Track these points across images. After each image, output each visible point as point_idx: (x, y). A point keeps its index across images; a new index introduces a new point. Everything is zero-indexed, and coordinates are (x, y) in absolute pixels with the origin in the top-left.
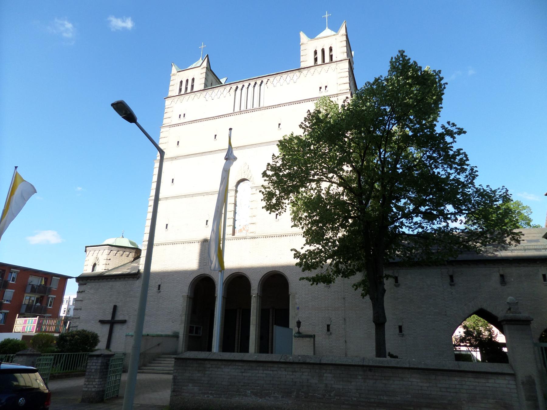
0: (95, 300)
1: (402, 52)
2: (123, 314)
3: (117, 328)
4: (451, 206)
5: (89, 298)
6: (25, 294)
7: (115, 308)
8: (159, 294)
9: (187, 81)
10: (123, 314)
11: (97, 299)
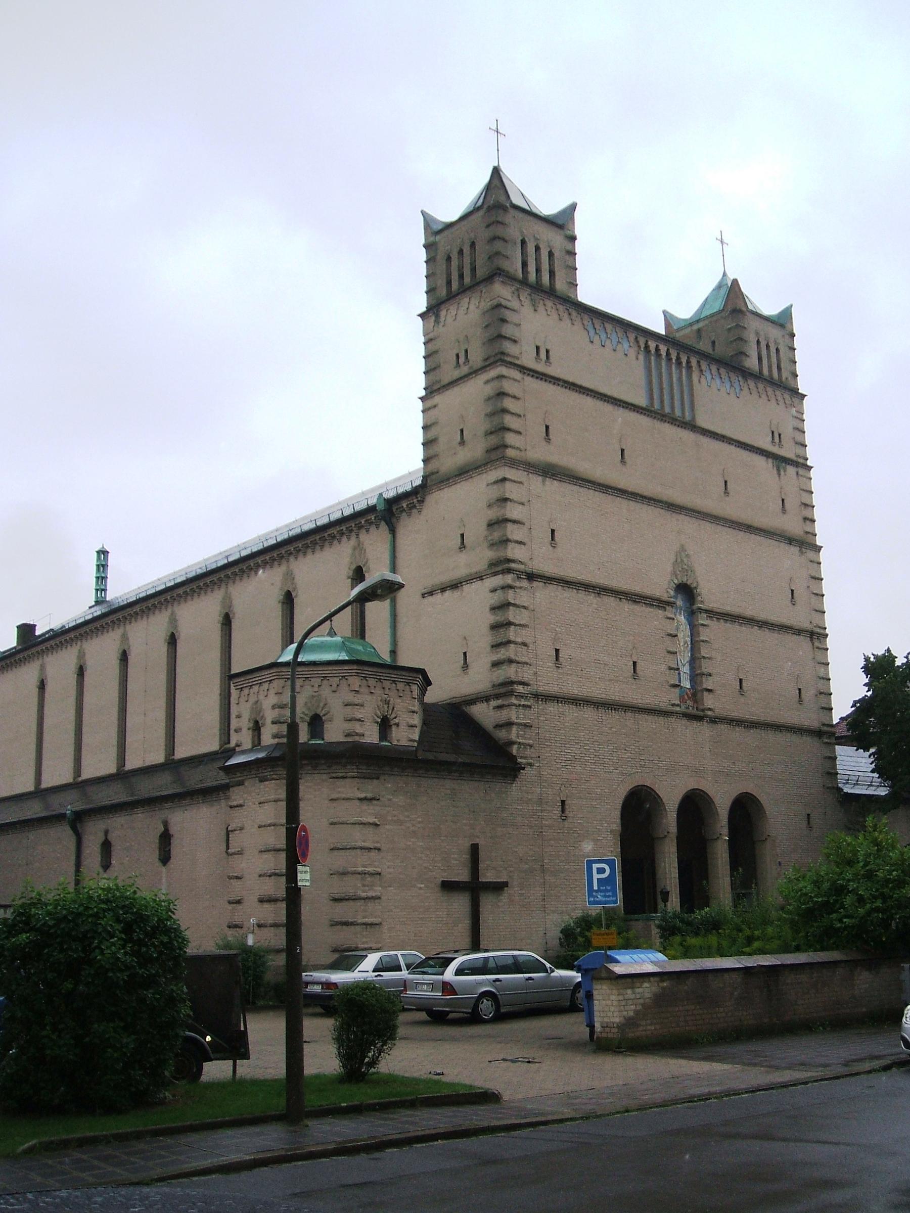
0: (413, 825)
1: (888, 650)
2: (494, 868)
3: (487, 903)
4: (883, 794)
5: (395, 818)
6: (393, 506)
7: (475, 850)
8: (566, 823)
9: (461, 252)
10: (494, 868)
11: (419, 822)
